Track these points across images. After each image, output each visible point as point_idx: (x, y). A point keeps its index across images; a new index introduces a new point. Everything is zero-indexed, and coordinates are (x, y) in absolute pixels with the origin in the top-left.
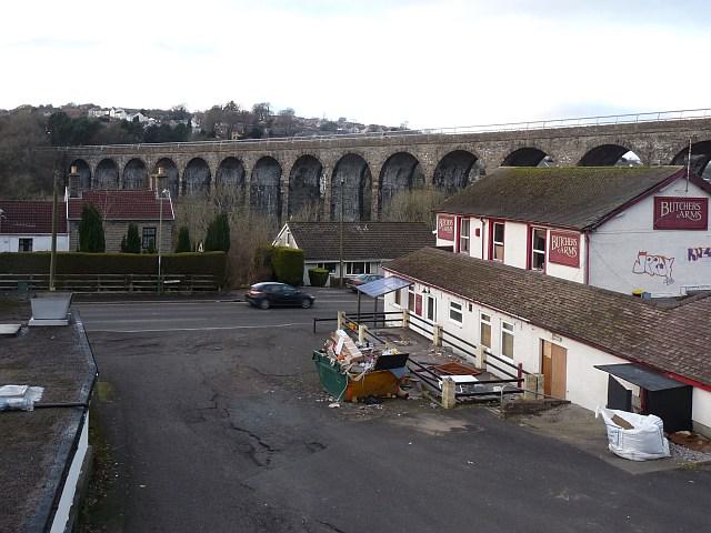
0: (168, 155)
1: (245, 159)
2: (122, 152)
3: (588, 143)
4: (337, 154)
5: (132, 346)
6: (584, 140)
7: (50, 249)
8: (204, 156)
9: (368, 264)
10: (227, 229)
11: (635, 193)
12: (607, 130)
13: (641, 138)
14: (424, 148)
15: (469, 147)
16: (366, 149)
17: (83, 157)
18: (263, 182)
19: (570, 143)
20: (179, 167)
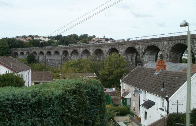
0: (22, 51)
1: (52, 52)
2: (52, 49)
3: (147, 44)
4: (72, 50)
5: (29, 80)
6: (125, 46)
7: (176, 112)
8: (42, 51)
9: (111, 107)
10: (34, 62)
11: (189, 90)
12: (143, 41)
13: (138, 45)
14: (91, 48)
15: (153, 44)
16: (78, 49)
17: (17, 51)
18: (57, 59)
19: (122, 46)
20: (37, 54)
